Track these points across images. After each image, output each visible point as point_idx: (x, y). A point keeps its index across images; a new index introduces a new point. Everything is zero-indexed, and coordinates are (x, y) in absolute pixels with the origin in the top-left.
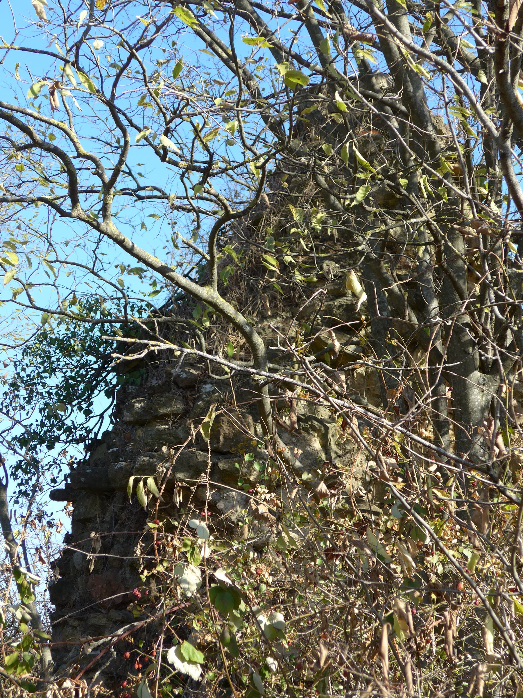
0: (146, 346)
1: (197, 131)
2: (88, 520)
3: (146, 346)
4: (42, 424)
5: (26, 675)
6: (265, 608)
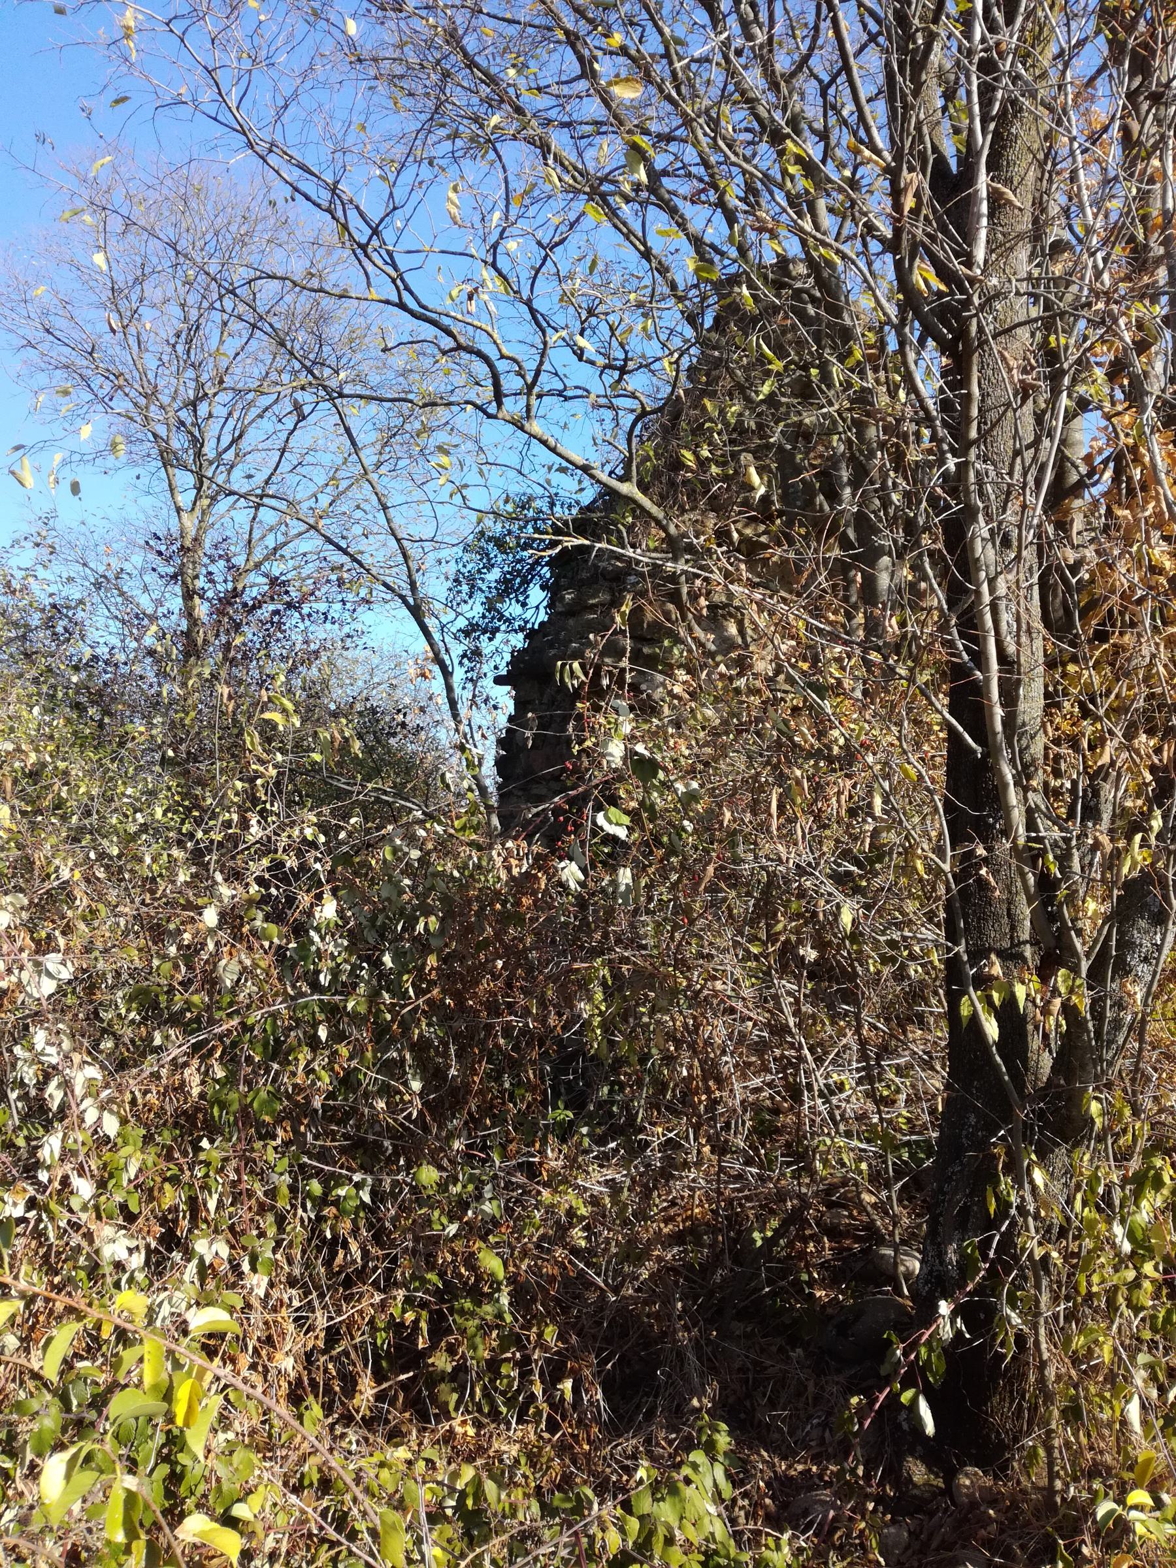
0: (559, 542)
1: (612, 329)
2: (529, 702)
3: (559, 542)
4: (484, 617)
5: (474, 837)
6: (682, 778)
